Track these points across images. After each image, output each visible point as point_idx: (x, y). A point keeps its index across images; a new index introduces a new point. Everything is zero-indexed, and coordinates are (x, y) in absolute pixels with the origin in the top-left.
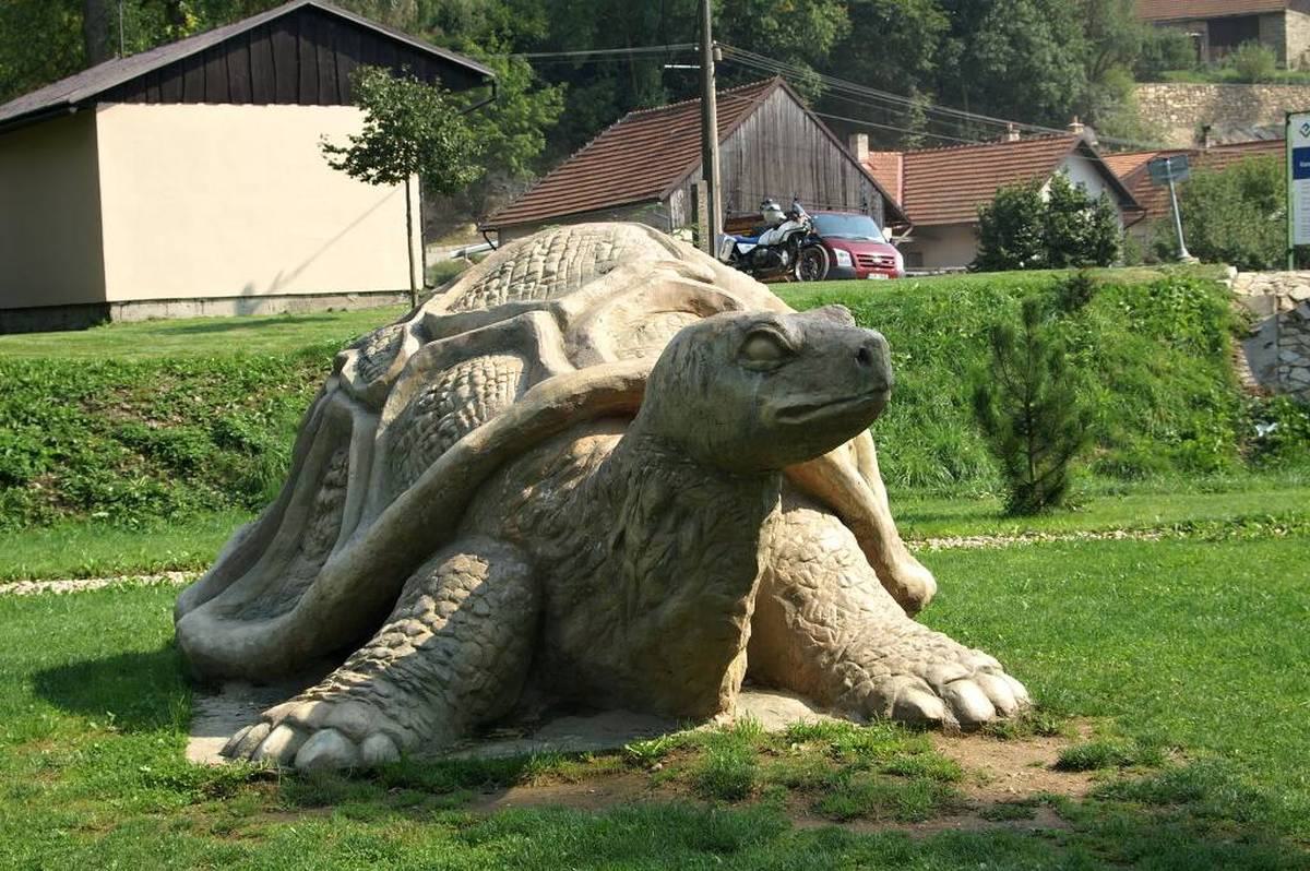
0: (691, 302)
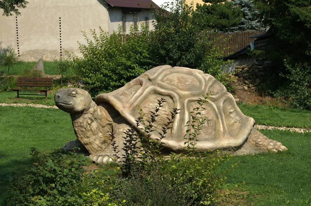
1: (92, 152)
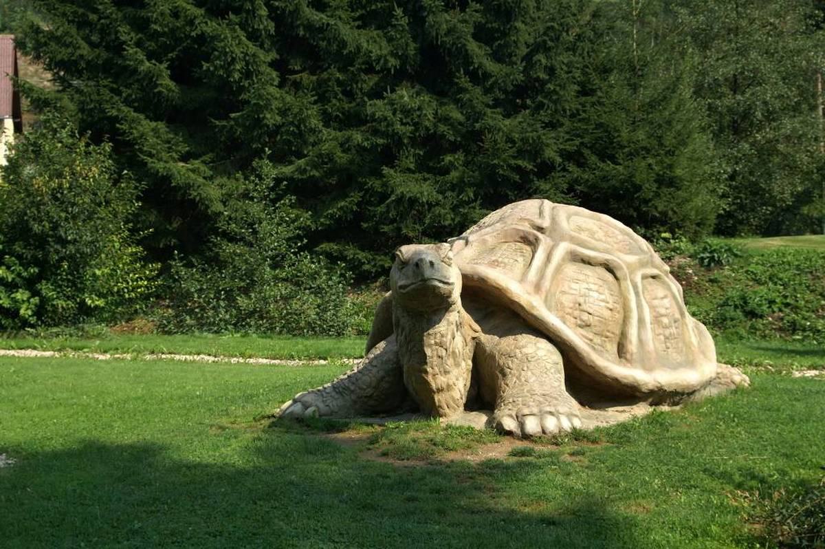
0: (522, 238)
1: (447, 410)
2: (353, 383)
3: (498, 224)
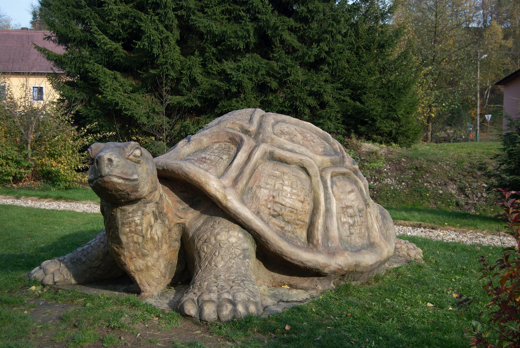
2: (85, 256)
3: (215, 128)
